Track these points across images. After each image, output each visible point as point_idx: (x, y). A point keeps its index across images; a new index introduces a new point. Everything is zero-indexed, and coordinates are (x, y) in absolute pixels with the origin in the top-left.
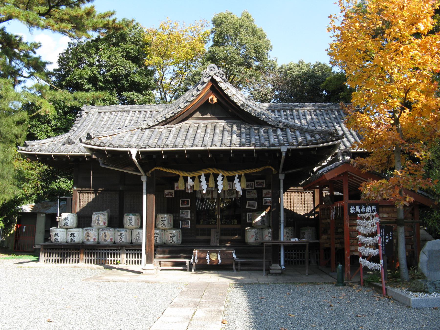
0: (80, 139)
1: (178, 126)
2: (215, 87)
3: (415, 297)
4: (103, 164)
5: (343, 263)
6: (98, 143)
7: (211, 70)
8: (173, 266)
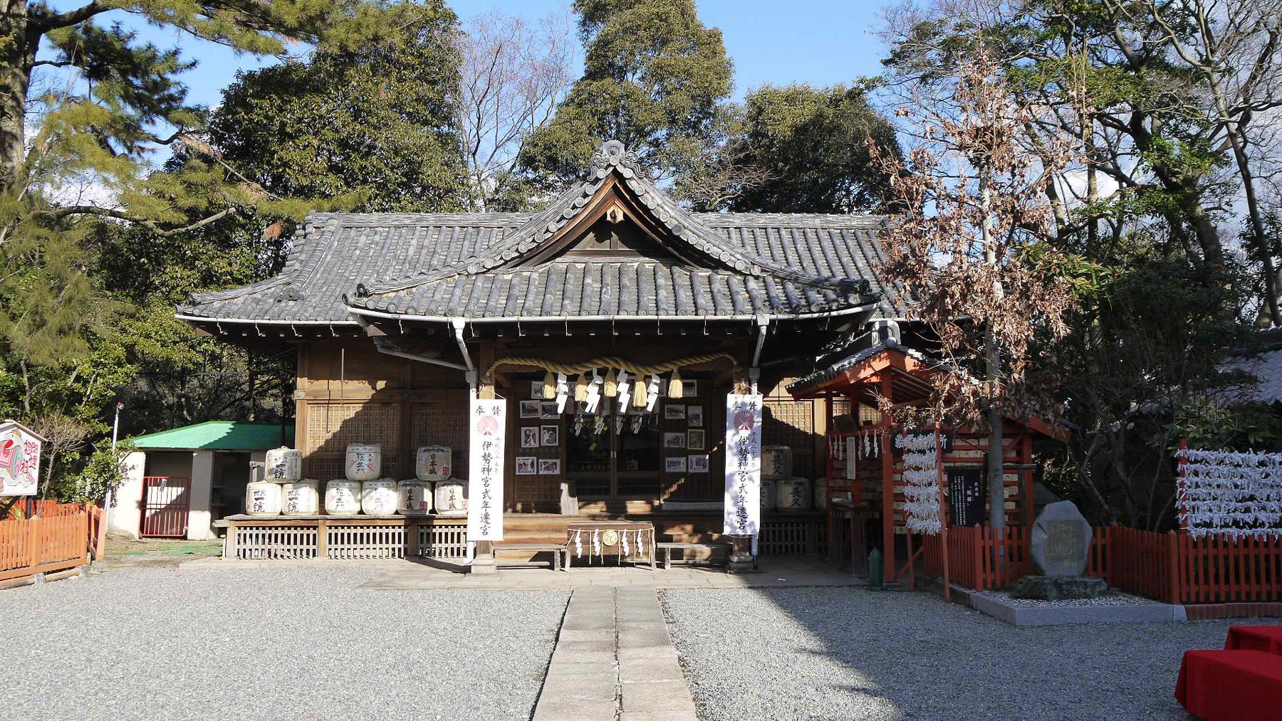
0: (344, 296)
1: (544, 268)
2: (621, 190)
3: (1021, 607)
4: (383, 347)
5: (881, 550)
6: (382, 305)
7: (612, 153)
8: (535, 559)
